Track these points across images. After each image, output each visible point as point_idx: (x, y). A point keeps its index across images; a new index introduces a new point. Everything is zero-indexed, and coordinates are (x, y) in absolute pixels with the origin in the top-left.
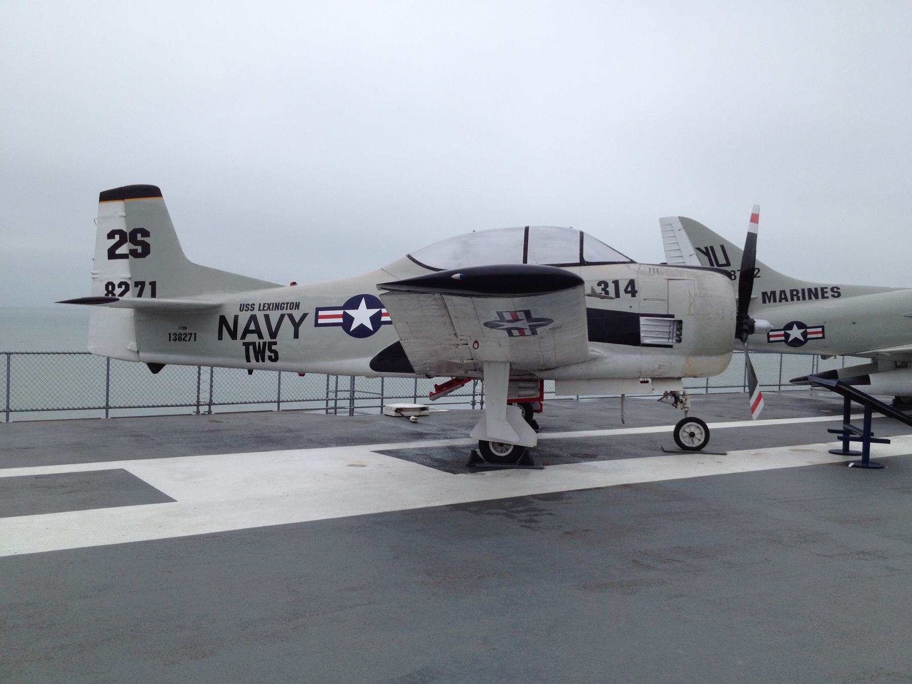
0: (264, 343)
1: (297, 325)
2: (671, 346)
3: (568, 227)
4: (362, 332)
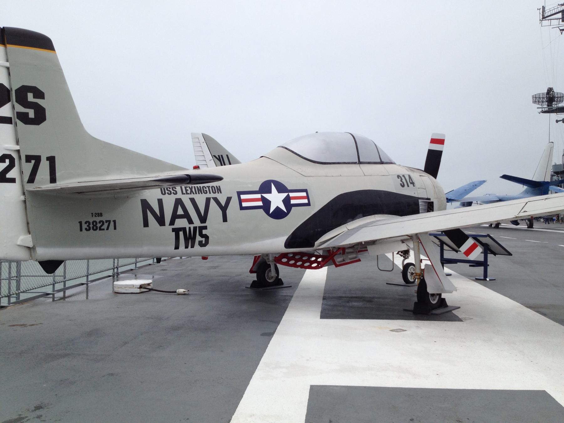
0: (195, 228)
1: (224, 209)
4: (278, 214)
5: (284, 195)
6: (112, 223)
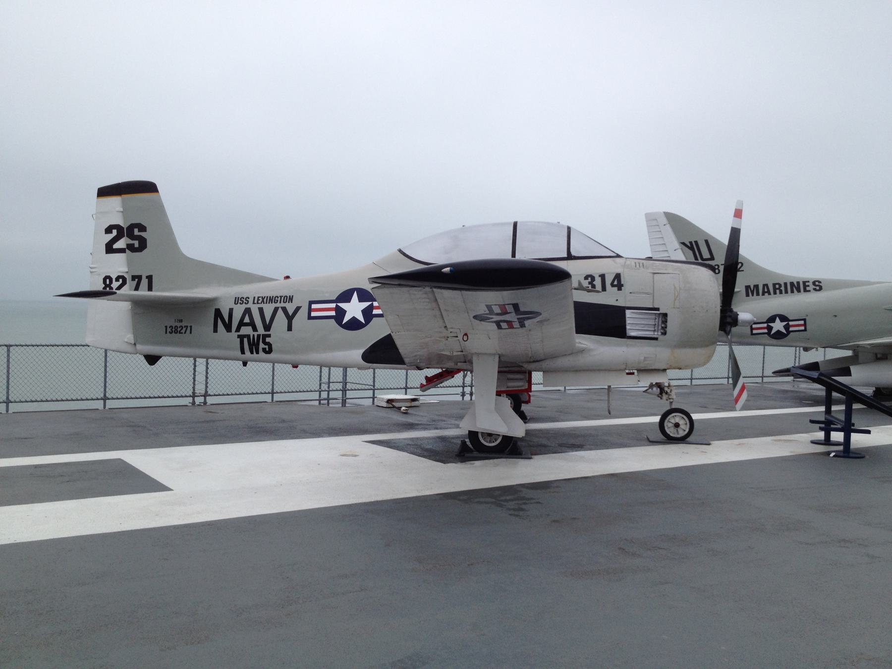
0: (259, 336)
1: (290, 318)
2: (656, 339)
3: (556, 222)
4: (354, 324)
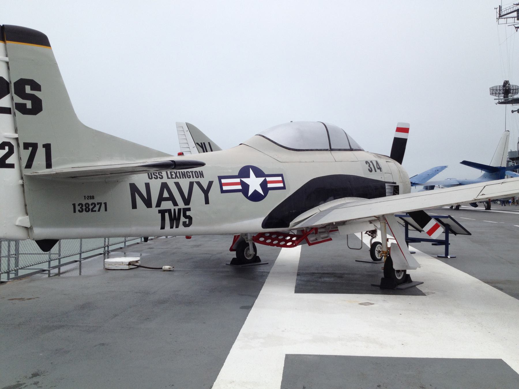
0: (179, 210)
1: (206, 192)
4: (256, 197)
5: (261, 179)
6: (103, 205)
